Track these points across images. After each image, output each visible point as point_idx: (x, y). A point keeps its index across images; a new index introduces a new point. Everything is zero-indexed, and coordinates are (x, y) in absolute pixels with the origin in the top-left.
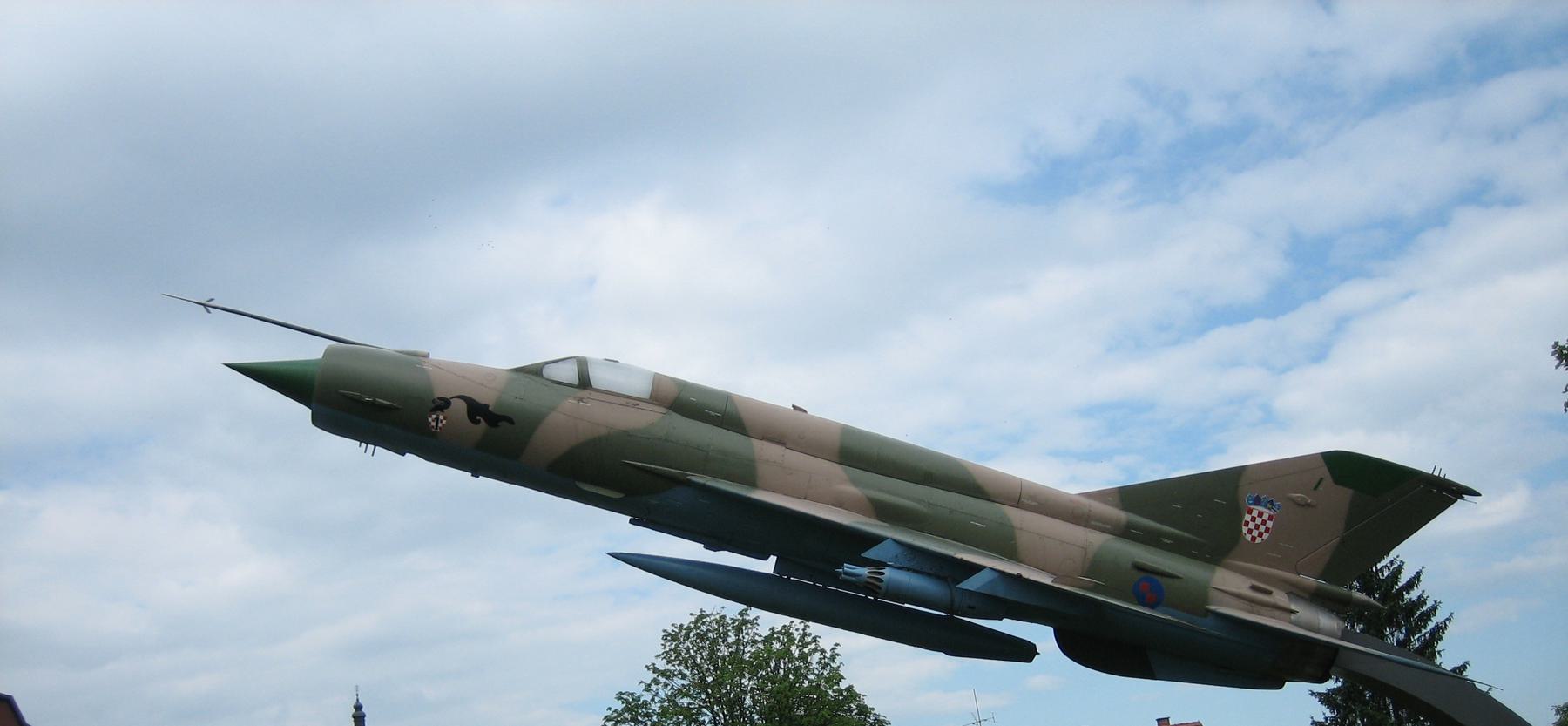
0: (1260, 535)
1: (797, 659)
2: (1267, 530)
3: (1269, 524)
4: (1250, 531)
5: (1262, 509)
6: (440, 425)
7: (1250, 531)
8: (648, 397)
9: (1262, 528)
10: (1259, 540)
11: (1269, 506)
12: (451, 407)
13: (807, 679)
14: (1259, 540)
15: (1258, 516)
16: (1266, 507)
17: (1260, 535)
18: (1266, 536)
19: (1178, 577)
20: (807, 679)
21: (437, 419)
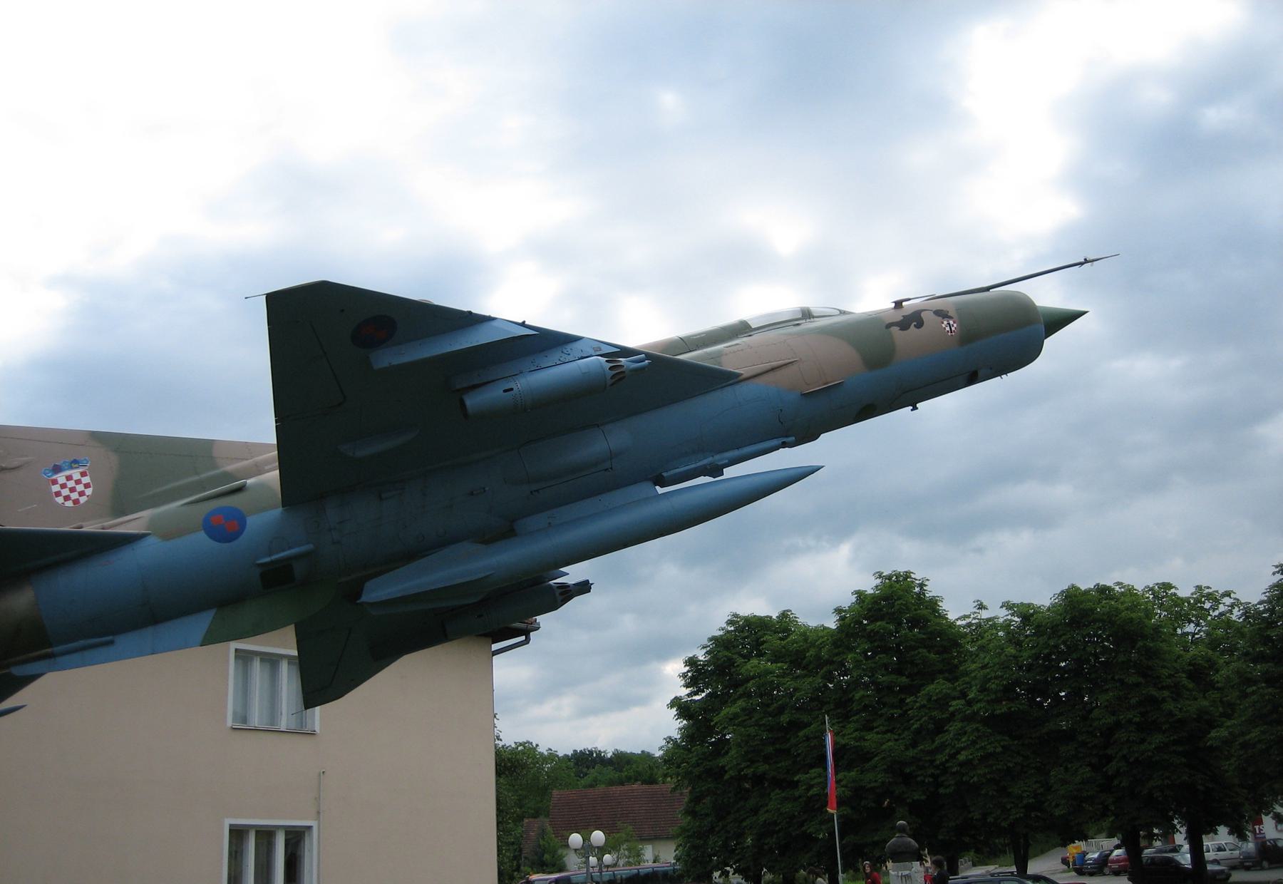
0: (67, 498)
1: (1193, 622)
2: (76, 502)
3: (86, 480)
4: (82, 494)
5: (68, 473)
6: (953, 329)
7: (82, 494)
8: (800, 316)
9: (74, 496)
10: (60, 500)
11: (74, 466)
12: (925, 324)
13: (1095, 651)
14: (60, 500)
15: (61, 485)
16: (72, 468)
17: (67, 498)
18: (69, 504)
19: (481, 635)
20: (1095, 651)
21: (949, 324)
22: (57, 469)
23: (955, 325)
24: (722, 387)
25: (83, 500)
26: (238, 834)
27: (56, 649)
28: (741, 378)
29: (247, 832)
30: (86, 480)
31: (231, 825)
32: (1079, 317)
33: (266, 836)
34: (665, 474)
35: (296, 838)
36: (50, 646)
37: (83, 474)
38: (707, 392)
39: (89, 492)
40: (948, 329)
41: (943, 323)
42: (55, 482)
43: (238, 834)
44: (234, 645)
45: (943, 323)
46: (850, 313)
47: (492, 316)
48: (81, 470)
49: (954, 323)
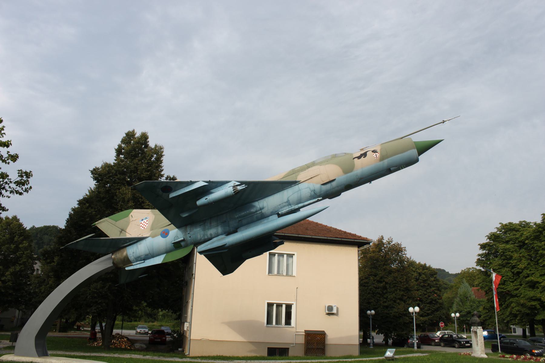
3: (147, 222)
6: (377, 156)
21: (376, 155)
22: (142, 220)
23: (378, 155)
24: (298, 184)
25: (146, 227)
26: (270, 305)
27: (133, 264)
28: (300, 182)
29: (273, 305)
30: (147, 222)
31: (267, 303)
32: (433, 147)
33: (279, 306)
34: (279, 213)
35: (289, 307)
36: (132, 263)
37: (147, 221)
38: (377, 173)
39: (147, 225)
40: (375, 156)
41: (374, 155)
42: (141, 223)
43: (270, 305)
44: (268, 253)
45: (374, 155)
46: (191, 183)
47: (192, 180)
48: (147, 220)
49: (378, 154)
